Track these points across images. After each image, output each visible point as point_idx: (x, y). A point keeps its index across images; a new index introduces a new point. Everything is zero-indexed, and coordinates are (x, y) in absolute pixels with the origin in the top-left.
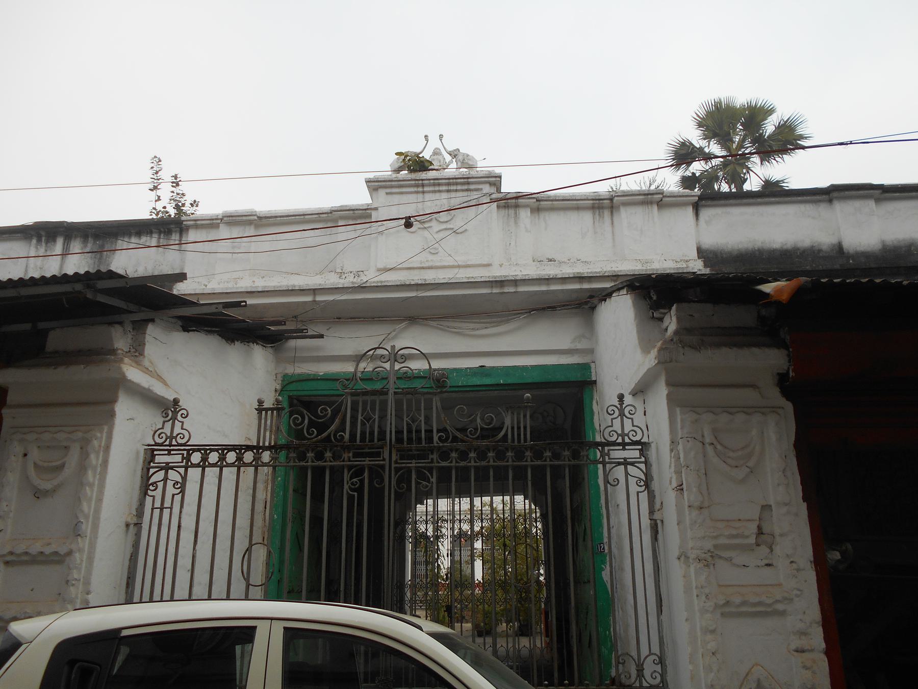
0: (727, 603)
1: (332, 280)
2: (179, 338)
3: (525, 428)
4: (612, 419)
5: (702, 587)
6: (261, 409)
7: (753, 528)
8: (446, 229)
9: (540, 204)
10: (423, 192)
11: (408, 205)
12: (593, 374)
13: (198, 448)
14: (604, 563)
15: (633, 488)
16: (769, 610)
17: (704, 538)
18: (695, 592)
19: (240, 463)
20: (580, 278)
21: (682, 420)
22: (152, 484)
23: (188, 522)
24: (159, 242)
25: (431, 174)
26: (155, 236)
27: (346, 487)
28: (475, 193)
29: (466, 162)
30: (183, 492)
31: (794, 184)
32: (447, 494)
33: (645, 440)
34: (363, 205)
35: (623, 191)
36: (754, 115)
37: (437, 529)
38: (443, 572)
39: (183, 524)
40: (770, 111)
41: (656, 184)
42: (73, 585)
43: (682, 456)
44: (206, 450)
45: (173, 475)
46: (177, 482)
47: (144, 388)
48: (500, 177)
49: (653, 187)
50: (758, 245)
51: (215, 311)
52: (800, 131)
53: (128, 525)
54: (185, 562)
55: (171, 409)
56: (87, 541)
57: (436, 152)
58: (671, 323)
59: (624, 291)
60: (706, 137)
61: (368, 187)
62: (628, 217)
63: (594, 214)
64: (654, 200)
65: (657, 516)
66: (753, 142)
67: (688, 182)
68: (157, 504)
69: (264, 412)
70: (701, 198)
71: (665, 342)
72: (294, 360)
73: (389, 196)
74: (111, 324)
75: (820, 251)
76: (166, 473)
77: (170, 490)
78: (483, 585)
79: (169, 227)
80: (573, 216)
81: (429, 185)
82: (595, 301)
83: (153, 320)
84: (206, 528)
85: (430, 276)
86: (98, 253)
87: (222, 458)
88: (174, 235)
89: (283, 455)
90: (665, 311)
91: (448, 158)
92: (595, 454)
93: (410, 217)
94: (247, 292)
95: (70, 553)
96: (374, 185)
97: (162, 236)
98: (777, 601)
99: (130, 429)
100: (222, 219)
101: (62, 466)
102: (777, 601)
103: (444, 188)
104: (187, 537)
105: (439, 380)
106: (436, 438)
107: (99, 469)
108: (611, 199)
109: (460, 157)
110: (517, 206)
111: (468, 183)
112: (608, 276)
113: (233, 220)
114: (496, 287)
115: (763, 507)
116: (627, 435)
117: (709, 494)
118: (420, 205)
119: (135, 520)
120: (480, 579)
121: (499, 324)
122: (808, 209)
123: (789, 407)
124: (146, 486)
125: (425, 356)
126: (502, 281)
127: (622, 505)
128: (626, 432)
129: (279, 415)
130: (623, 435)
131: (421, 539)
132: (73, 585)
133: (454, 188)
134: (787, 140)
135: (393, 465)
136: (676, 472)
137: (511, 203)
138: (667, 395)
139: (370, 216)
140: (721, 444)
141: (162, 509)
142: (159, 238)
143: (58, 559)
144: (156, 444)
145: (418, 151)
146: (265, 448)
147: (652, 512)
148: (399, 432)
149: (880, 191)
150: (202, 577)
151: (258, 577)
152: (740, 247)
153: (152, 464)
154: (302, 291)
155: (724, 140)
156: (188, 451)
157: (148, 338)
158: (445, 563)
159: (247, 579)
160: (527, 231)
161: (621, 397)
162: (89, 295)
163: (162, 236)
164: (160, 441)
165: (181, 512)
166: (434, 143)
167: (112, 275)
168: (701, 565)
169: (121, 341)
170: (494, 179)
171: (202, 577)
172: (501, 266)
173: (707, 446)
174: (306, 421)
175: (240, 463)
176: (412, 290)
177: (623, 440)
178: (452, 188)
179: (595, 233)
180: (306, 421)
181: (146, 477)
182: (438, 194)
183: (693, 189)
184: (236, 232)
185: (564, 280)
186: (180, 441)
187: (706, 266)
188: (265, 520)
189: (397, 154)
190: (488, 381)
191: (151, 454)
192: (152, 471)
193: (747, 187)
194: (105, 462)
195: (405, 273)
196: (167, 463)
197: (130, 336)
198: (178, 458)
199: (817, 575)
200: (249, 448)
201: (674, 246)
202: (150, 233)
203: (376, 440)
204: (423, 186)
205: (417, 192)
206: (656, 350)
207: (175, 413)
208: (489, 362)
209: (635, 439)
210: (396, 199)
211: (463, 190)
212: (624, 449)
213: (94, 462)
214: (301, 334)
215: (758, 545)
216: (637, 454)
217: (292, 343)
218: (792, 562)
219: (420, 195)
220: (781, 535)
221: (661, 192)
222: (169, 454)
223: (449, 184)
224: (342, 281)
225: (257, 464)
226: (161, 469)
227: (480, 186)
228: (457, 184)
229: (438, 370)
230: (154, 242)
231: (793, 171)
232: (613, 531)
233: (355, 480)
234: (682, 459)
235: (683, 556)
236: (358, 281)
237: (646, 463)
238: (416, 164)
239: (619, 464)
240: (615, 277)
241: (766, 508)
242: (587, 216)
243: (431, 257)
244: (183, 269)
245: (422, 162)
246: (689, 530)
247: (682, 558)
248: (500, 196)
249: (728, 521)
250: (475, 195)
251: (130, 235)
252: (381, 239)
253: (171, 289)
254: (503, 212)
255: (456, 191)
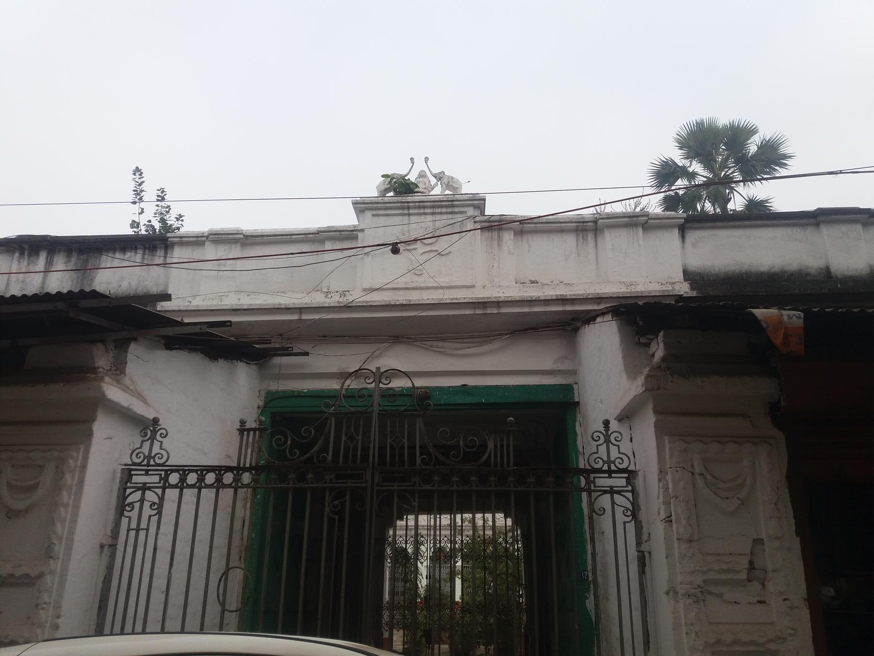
0: (718, 642)
1: (318, 299)
2: (162, 356)
3: (508, 446)
4: (598, 446)
5: (692, 624)
6: (243, 430)
7: (744, 562)
8: (431, 251)
9: (525, 227)
10: (409, 215)
11: (393, 228)
12: (576, 395)
13: (177, 469)
14: (588, 591)
15: (620, 517)
16: (761, 649)
17: (693, 572)
18: (684, 629)
19: (219, 485)
20: (563, 300)
21: (670, 449)
22: (129, 505)
23: (165, 542)
24: (143, 258)
25: (416, 198)
26: (140, 252)
27: (327, 509)
28: (459, 216)
29: (450, 184)
30: (160, 513)
31: (780, 206)
32: (428, 511)
33: (632, 468)
34: (349, 226)
35: (607, 214)
36: (737, 136)
37: (417, 544)
38: (422, 591)
39: (159, 544)
40: (752, 132)
41: (641, 206)
42: (43, 609)
43: (670, 487)
44: (184, 471)
45: (150, 496)
46: (154, 503)
47: (123, 407)
48: (484, 200)
49: (638, 210)
50: (746, 268)
51: (199, 331)
52: (784, 150)
53: (102, 547)
54: (160, 583)
55: (150, 428)
56: (59, 564)
57: (422, 175)
58: (658, 350)
59: (609, 317)
60: (688, 157)
61: (355, 208)
62: (611, 240)
63: (577, 237)
64: (637, 222)
65: (645, 547)
66: (737, 162)
67: (671, 203)
68: (134, 525)
69: (245, 433)
70: (688, 220)
71: (652, 369)
72: (278, 377)
73: (376, 218)
74: (93, 342)
75: (808, 274)
76: (143, 494)
77: (147, 511)
78: (465, 607)
79: (155, 243)
80: (557, 239)
81: (415, 208)
82: (579, 324)
83: (135, 339)
84: (183, 548)
85: (415, 297)
86: (83, 270)
87: (201, 479)
88: (158, 251)
89: (263, 476)
90: (652, 337)
91: (433, 181)
92: (579, 481)
93: (397, 243)
94: (233, 310)
95: (41, 575)
96: (362, 206)
97: (147, 252)
98: (771, 641)
99: (107, 448)
100: (207, 237)
101: (34, 487)
102: (771, 641)
103: (429, 211)
104: (163, 558)
105: (423, 397)
106: (418, 461)
107: (74, 490)
108: (595, 222)
109: (445, 180)
110: (500, 229)
111: (453, 206)
112: (591, 299)
113: (220, 238)
114: (479, 308)
115: (754, 540)
116: (614, 462)
117: (699, 526)
118: (405, 227)
119: (110, 542)
120: (457, 579)
121: (480, 344)
122: (796, 232)
123: (781, 437)
124: (122, 506)
125: (406, 374)
126: (485, 303)
127: (611, 537)
128: (612, 459)
129: (261, 436)
130: (609, 462)
131: (401, 555)
132: (43, 609)
133: (439, 210)
134: (769, 160)
135: (376, 488)
136: (664, 503)
137: (496, 226)
138: (655, 424)
139: (356, 238)
140: (712, 475)
141: (138, 530)
142: (144, 254)
143: (29, 581)
144: (134, 464)
145: (404, 173)
146: (245, 469)
147: (639, 543)
148: (382, 448)
149: (867, 216)
150: (174, 611)
151: (234, 601)
152: (727, 269)
153: (129, 484)
154: (288, 310)
155: (708, 161)
156: (166, 471)
157: (130, 356)
158: (423, 582)
159: (223, 604)
160: (509, 253)
161: (606, 423)
162: (71, 314)
163: (147, 252)
164: (138, 461)
165: (157, 534)
166: (420, 166)
167: (95, 294)
168: (690, 601)
169: (102, 360)
170: (478, 202)
171: (174, 611)
172: (484, 287)
173: (697, 476)
174: (289, 442)
175: (219, 485)
176: (398, 311)
177: (609, 467)
178: (437, 210)
179: (579, 255)
180: (289, 442)
181: (122, 497)
182: (423, 217)
183: (676, 210)
184: (222, 251)
185: (547, 302)
186: (158, 461)
187: (692, 288)
188: (242, 539)
189: (383, 176)
190: (469, 400)
191: (127, 474)
192: (128, 491)
193: (731, 206)
194: (81, 482)
195: (390, 293)
196: (145, 484)
197: (112, 354)
198: (156, 479)
199: (811, 613)
200: (229, 469)
201: (657, 269)
202: (135, 249)
203: (359, 461)
204: (408, 208)
205: (403, 215)
206: (643, 377)
207: (154, 432)
208: (471, 381)
209: (621, 467)
210: (382, 221)
211: (447, 213)
212: (610, 477)
213: (69, 482)
214: (286, 352)
215: (749, 580)
216: (623, 482)
217: (277, 360)
218: (785, 600)
219: (406, 218)
220: (774, 571)
221: (647, 215)
222: (147, 474)
223: (433, 207)
224: (328, 300)
225: (236, 486)
226: (138, 489)
227: (464, 209)
228: (442, 207)
229: (421, 388)
230: (138, 258)
231: (781, 194)
232: (598, 559)
233: (336, 502)
234: (670, 490)
235: (672, 591)
236: (344, 300)
237: (633, 492)
238: (401, 187)
239: (605, 492)
240: (599, 299)
241: (758, 541)
242: (570, 241)
243: (418, 279)
244: (167, 286)
245: (408, 184)
246: (678, 564)
247: (671, 593)
248: (484, 218)
249: (719, 555)
250: (459, 218)
251: (114, 251)
252: (368, 259)
253: (155, 306)
254: (487, 234)
255: (441, 213)
